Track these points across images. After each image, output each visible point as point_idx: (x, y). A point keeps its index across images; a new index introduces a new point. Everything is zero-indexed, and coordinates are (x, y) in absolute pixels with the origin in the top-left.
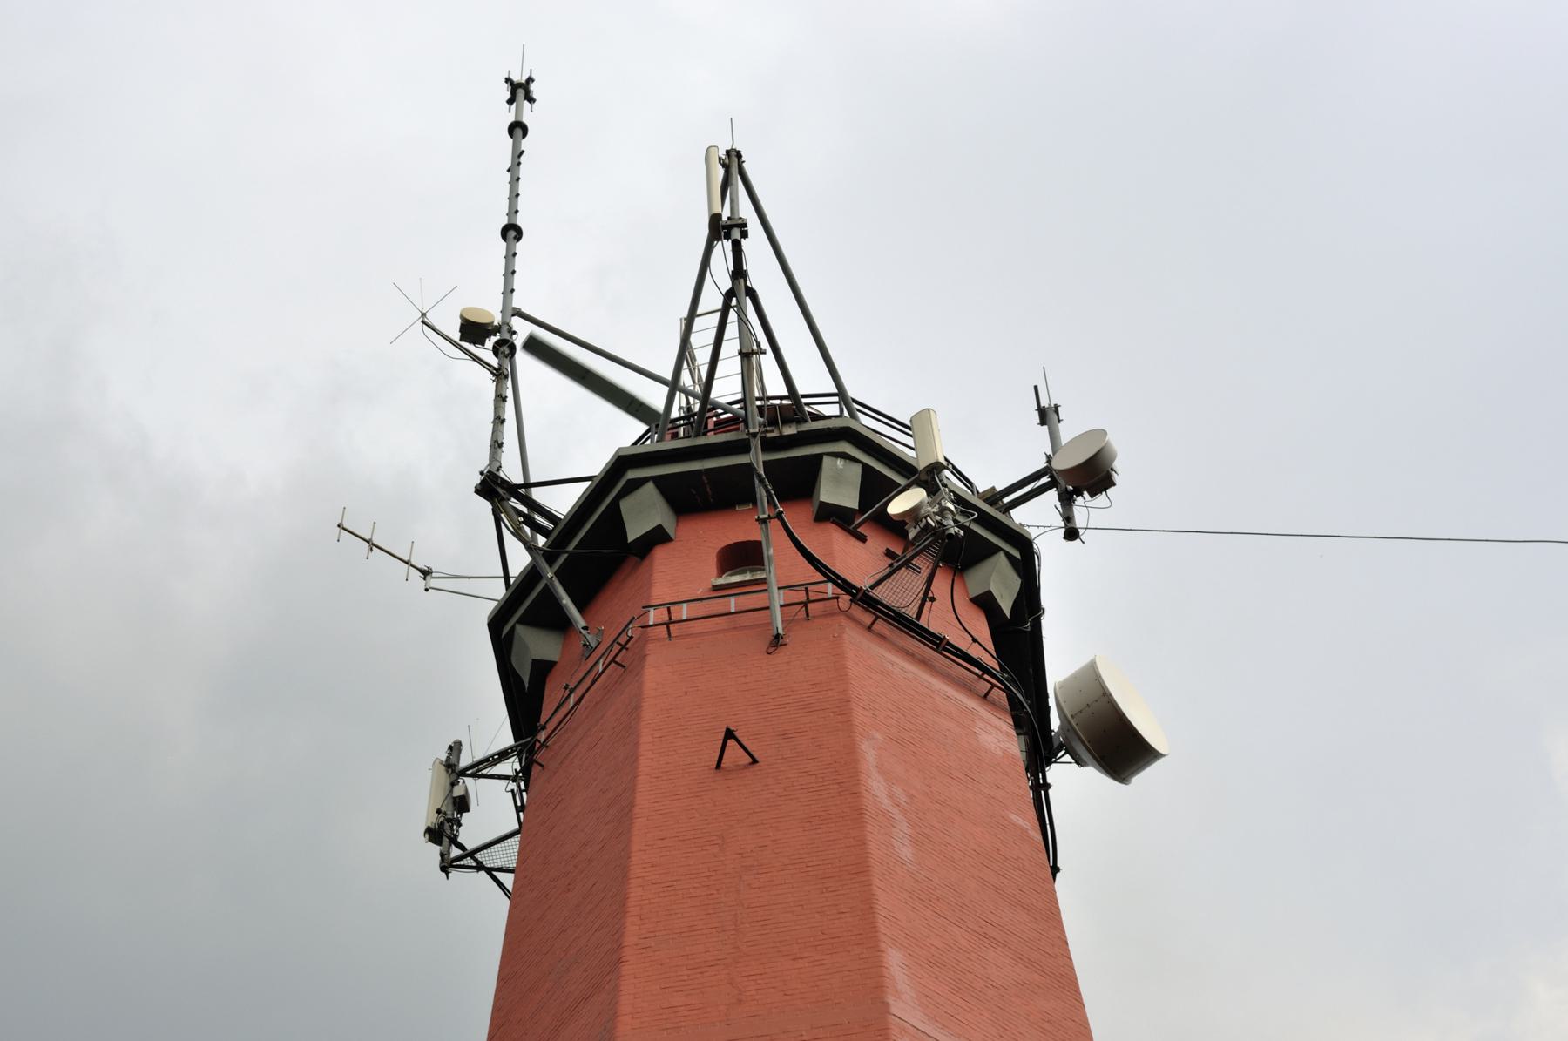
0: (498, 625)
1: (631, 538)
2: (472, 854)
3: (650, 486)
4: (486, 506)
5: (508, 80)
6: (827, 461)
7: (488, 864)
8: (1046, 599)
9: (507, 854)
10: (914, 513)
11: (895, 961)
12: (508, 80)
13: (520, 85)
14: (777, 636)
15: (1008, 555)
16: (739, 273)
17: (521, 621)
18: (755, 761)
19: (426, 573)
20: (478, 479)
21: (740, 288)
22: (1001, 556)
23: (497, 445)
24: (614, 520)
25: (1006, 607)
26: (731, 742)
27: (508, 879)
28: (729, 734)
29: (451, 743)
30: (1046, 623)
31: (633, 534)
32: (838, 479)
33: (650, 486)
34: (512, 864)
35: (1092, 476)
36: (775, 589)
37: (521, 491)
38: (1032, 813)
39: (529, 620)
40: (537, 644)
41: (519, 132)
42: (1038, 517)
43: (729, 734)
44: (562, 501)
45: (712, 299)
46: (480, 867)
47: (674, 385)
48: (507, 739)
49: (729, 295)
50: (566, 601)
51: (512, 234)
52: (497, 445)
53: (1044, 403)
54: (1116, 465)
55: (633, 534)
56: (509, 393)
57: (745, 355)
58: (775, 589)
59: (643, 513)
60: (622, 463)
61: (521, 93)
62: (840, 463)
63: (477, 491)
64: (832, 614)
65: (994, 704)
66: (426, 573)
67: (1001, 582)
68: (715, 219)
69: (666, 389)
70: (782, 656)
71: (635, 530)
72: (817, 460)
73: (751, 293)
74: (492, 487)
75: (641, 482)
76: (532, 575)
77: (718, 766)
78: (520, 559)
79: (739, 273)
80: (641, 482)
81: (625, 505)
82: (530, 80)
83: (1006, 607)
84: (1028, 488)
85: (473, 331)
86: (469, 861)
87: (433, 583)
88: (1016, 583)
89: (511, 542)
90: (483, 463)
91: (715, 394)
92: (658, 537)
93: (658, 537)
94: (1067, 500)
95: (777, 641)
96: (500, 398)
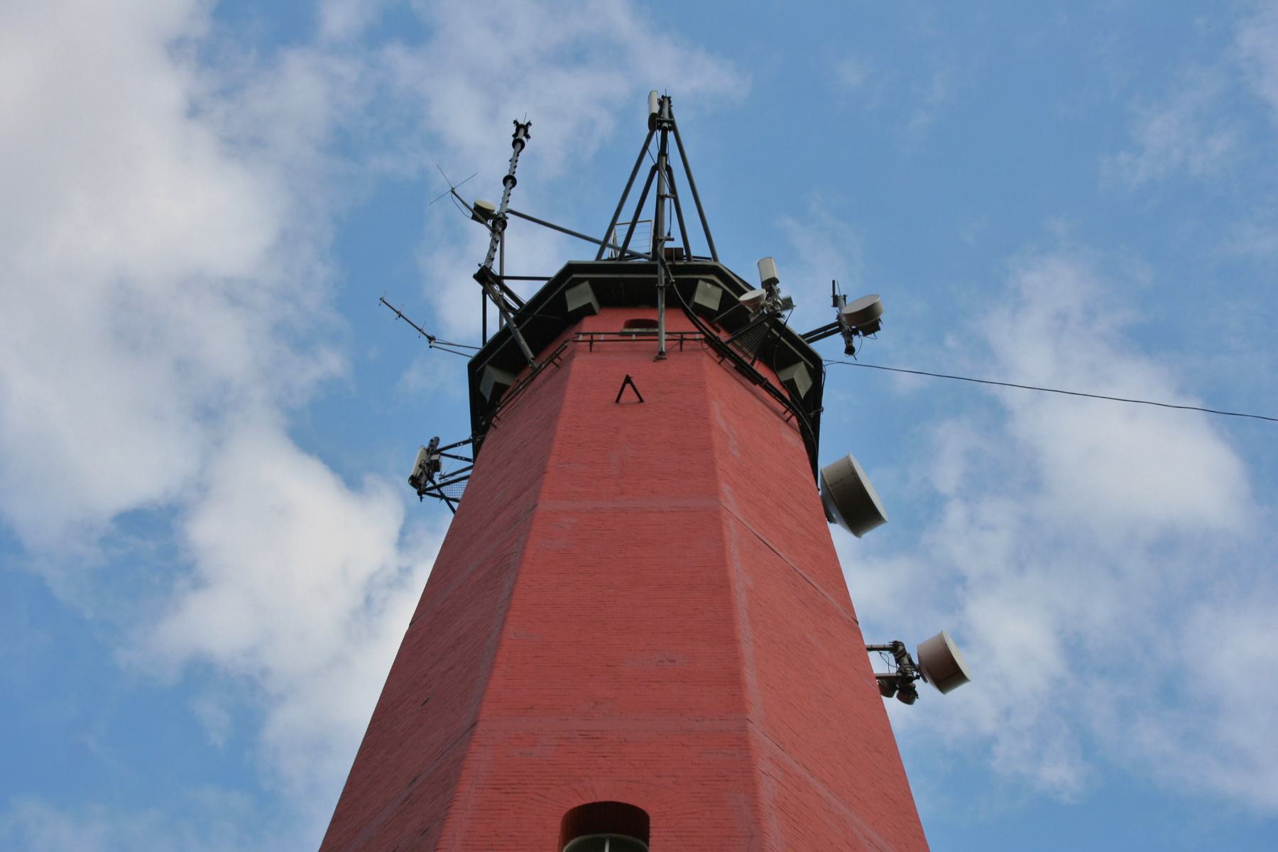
0: (475, 369)
1: (570, 309)
2: (438, 487)
3: (586, 284)
4: (479, 288)
5: (515, 122)
6: (701, 283)
7: (447, 495)
9: (457, 491)
10: (755, 301)
11: (726, 488)
12: (515, 122)
13: (522, 126)
14: (661, 353)
15: (806, 365)
16: (663, 153)
17: (490, 363)
18: (641, 400)
19: (431, 339)
22: (802, 365)
23: (491, 259)
24: (562, 300)
25: (803, 392)
26: (628, 386)
27: (455, 505)
28: (628, 380)
29: (432, 437)
30: (823, 416)
31: (571, 307)
32: (707, 293)
33: (586, 284)
34: (459, 497)
36: (664, 337)
37: (499, 279)
40: (494, 376)
41: (509, 183)
42: (829, 349)
43: (628, 380)
44: (526, 292)
45: (648, 163)
46: (442, 496)
48: (468, 434)
49: (654, 169)
50: (523, 342)
51: (509, 181)
52: (491, 259)
53: (837, 293)
54: (882, 317)
55: (571, 307)
56: (498, 248)
57: (661, 198)
58: (664, 337)
59: (579, 297)
60: (571, 269)
61: (522, 132)
62: (709, 286)
63: (475, 277)
64: (697, 350)
65: (791, 426)
66: (431, 339)
69: (598, 247)
70: (661, 364)
72: (696, 281)
73: (669, 169)
74: (484, 276)
75: (581, 281)
76: (504, 333)
77: (618, 401)
78: (494, 329)
79: (663, 153)
80: (583, 280)
81: (568, 294)
82: (529, 124)
83: (803, 392)
85: (481, 214)
86: (436, 492)
87: (433, 343)
88: (810, 383)
89: (490, 304)
90: (483, 261)
92: (587, 311)
93: (587, 311)
94: (848, 336)
95: (661, 356)
96: (493, 249)
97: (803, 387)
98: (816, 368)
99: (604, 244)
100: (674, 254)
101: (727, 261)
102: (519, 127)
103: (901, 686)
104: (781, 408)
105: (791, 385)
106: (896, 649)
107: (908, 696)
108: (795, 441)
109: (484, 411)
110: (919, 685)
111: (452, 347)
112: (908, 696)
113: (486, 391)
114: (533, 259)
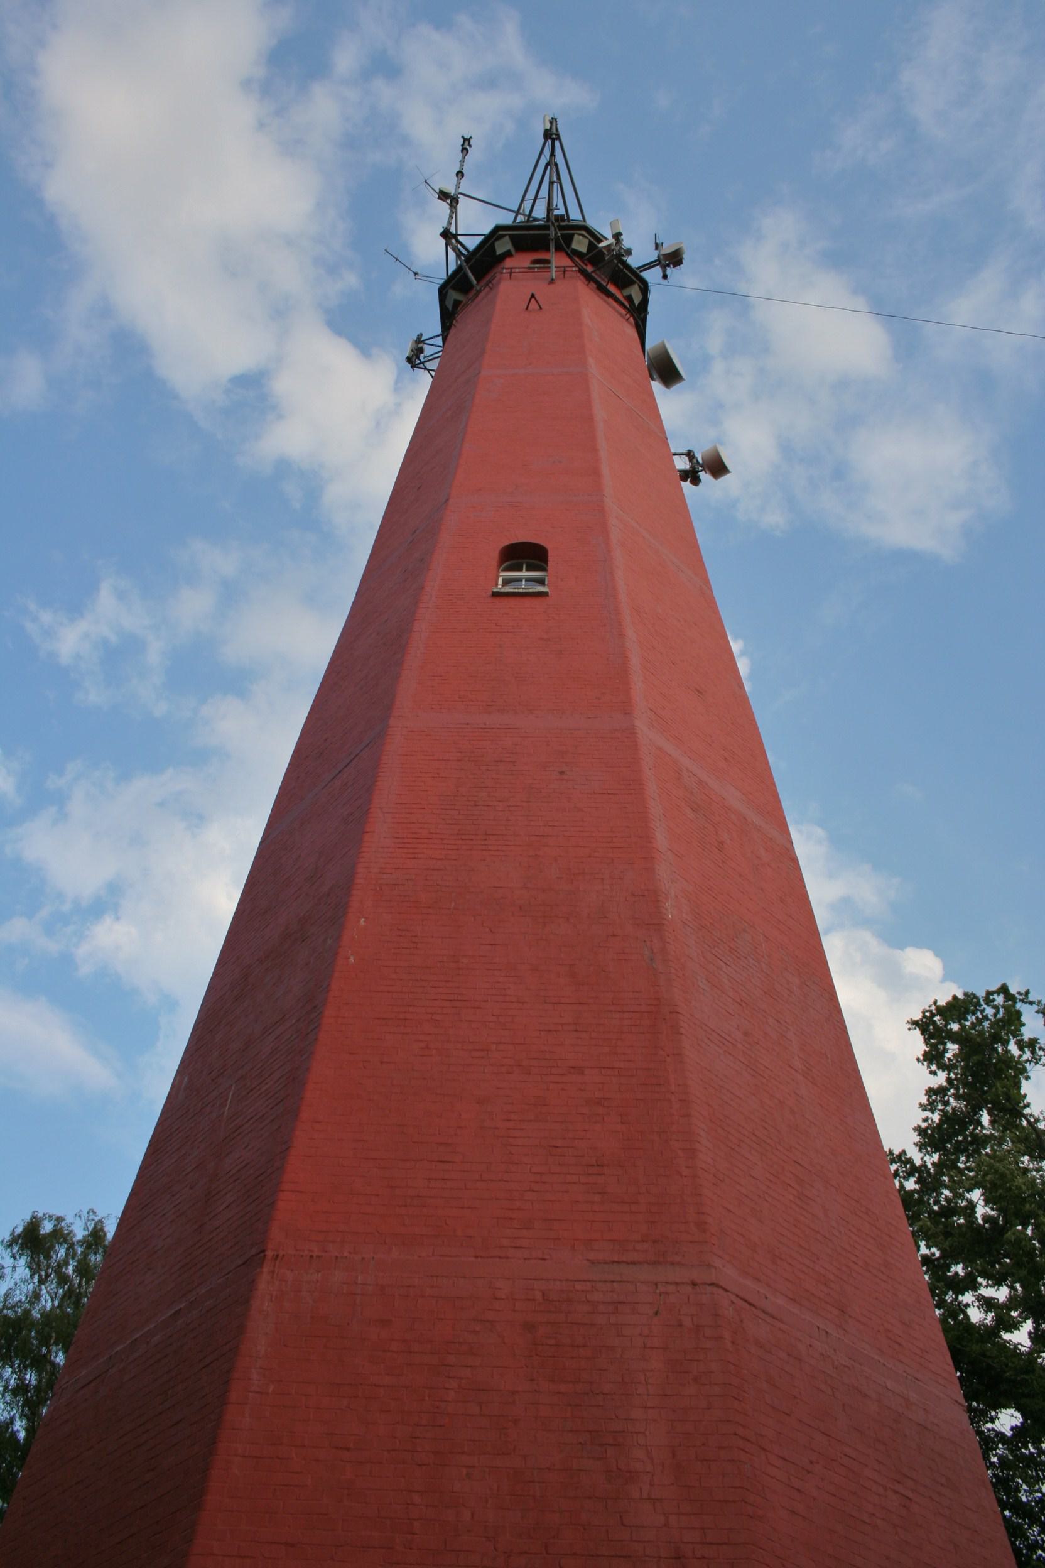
0: (443, 291)
3: (507, 238)
8: (651, 307)
9: (434, 365)
16: (552, 154)
19: (416, 274)
20: (441, 230)
21: (551, 164)
24: (493, 249)
25: (637, 302)
28: (533, 296)
32: (579, 242)
35: (674, 259)
38: (506, 600)
39: (454, 288)
40: (453, 295)
42: (652, 276)
43: (533, 296)
44: (472, 243)
46: (425, 368)
47: (517, 213)
48: (439, 330)
50: (470, 274)
59: (503, 246)
60: (498, 228)
66: (416, 274)
67: (635, 292)
68: (546, 131)
70: (552, 286)
71: (499, 251)
72: (573, 235)
73: (556, 165)
74: (446, 234)
75: (504, 236)
76: (459, 269)
79: (552, 154)
80: (504, 236)
83: (637, 302)
84: (649, 266)
85: (443, 195)
88: (641, 297)
91: (534, 214)
92: (508, 254)
93: (508, 254)
94: (664, 267)
97: (637, 299)
98: (645, 288)
99: (517, 213)
100: (559, 218)
101: (591, 223)
102: (465, 140)
103: (692, 476)
104: (624, 312)
105: (629, 298)
106: (690, 455)
107: (696, 481)
108: (632, 333)
109: (448, 317)
110: (703, 475)
111: (426, 278)
112: (696, 481)
113: (449, 304)
114: (476, 222)
